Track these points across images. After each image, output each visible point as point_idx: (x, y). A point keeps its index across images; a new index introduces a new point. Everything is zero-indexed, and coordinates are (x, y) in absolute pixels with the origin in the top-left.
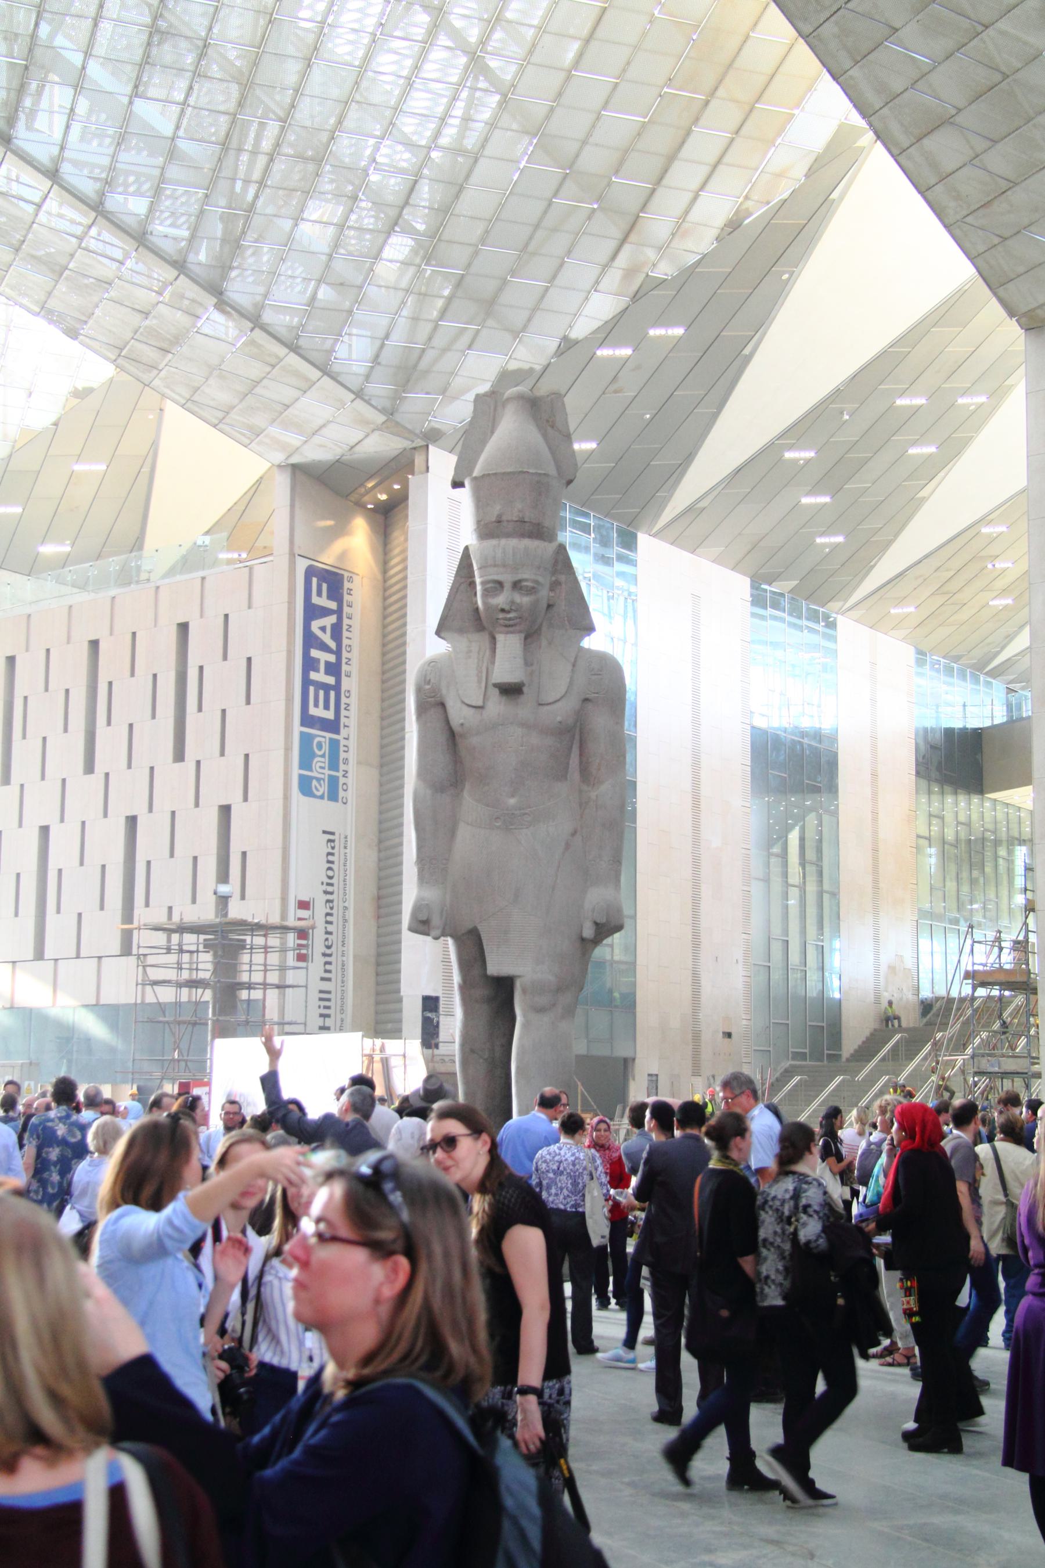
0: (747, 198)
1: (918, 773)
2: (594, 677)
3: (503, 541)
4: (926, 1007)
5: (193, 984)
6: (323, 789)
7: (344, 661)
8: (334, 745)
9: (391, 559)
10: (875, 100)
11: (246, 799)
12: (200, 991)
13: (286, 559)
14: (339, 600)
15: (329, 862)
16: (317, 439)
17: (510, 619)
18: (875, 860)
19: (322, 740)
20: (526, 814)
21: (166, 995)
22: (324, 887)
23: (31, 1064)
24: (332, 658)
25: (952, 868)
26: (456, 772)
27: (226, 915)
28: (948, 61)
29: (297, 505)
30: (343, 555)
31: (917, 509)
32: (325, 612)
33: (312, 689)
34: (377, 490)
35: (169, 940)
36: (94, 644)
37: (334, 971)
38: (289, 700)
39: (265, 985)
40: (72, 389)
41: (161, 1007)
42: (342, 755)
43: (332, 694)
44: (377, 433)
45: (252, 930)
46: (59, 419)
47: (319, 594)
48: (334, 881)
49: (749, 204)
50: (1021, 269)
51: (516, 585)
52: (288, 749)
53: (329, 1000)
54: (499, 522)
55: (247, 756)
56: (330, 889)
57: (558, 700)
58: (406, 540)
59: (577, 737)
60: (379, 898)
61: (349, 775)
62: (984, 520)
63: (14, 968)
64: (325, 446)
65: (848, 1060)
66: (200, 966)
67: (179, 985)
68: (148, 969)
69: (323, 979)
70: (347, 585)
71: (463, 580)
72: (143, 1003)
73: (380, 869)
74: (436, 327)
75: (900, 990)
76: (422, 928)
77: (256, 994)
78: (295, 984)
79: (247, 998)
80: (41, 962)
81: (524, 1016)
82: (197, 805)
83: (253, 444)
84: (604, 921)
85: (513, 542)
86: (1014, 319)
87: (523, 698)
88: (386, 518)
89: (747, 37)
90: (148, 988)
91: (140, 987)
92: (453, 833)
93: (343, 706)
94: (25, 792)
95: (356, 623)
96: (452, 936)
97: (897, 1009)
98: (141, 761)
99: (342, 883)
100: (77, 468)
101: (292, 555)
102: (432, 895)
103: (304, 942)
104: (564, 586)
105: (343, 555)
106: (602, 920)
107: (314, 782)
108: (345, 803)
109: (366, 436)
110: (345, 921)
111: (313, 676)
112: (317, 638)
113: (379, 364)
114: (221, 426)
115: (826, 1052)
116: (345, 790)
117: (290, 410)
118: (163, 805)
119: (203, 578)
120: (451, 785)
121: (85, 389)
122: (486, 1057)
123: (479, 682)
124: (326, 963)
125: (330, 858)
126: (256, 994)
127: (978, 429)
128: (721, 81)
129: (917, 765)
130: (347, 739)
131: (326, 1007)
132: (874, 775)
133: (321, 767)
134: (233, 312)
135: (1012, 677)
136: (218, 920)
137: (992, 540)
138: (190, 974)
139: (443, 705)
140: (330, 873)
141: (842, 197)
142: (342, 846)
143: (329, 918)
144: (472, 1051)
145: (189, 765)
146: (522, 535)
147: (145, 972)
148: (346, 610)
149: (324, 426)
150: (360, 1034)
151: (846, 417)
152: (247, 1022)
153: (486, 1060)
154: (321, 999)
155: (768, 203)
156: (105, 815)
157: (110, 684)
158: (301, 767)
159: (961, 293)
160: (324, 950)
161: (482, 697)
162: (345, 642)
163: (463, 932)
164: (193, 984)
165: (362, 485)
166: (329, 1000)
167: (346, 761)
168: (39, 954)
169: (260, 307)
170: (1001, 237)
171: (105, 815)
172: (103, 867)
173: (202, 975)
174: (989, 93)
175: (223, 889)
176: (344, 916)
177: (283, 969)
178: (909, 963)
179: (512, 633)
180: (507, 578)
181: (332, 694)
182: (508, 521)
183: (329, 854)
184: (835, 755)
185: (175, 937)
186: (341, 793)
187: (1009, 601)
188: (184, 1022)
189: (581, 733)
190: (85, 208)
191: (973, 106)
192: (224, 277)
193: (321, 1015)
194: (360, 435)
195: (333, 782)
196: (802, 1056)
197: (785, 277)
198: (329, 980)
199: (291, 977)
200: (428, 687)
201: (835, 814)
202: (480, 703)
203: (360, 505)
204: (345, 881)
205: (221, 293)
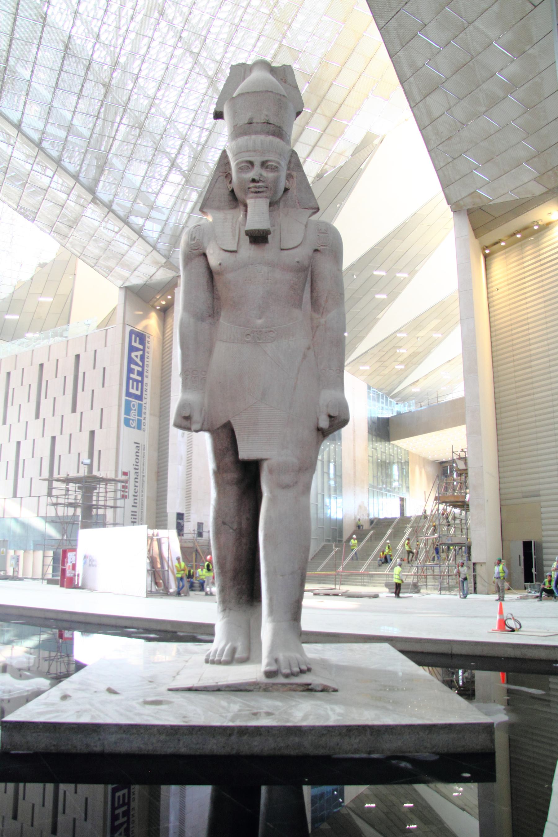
0: (326, 164)
2: (321, 235)
3: (253, 137)
4: (372, 522)
6: (135, 424)
7: (145, 371)
8: (140, 406)
9: (166, 334)
10: (408, 72)
11: (101, 428)
13: (121, 326)
15: (137, 456)
16: (136, 273)
17: (259, 187)
18: (354, 464)
19: (135, 403)
20: (271, 331)
21: (61, 511)
24: (140, 369)
25: (380, 469)
26: (213, 307)
28: (447, 47)
29: (127, 304)
30: (146, 327)
31: (376, 323)
32: (138, 350)
33: (131, 381)
34: (160, 299)
36: (42, 365)
37: (138, 503)
38: (121, 385)
39: (105, 507)
40: (38, 263)
42: (144, 411)
43: (140, 384)
44: (162, 268)
45: (100, 481)
46: (33, 276)
47: (135, 342)
48: (139, 464)
49: (327, 167)
50: (458, 177)
51: (264, 164)
52: (120, 406)
53: (135, 515)
54: (251, 123)
55: (102, 409)
56: (137, 467)
57: (296, 247)
58: (173, 321)
59: (309, 279)
60: (158, 472)
61: (147, 419)
62: (399, 331)
63: (5, 500)
64: (139, 277)
69: (133, 506)
70: (147, 339)
71: (221, 174)
73: (159, 460)
74: (189, 217)
75: (363, 515)
76: (185, 423)
77: (101, 512)
79: (64, 491)
80: (15, 499)
81: (271, 492)
82: (81, 431)
83: (109, 277)
85: (261, 138)
86: (449, 206)
88: (165, 314)
89: (332, 84)
92: (210, 352)
93: (144, 390)
94: (12, 427)
95: (151, 355)
97: (361, 523)
98: (58, 413)
99: (142, 465)
100: (41, 299)
101: (124, 324)
102: (193, 397)
104: (295, 179)
105: (146, 327)
107: (131, 421)
108: (144, 431)
109: (157, 270)
110: (143, 481)
111: (132, 376)
112: (134, 360)
113: (164, 233)
114: (95, 267)
115: (337, 539)
116: (144, 426)
117: (125, 257)
118: (66, 431)
120: (210, 316)
121: (44, 263)
123: (234, 236)
125: (138, 454)
126: (101, 512)
127: (403, 289)
128: (319, 105)
129: (368, 428)
130: (145, 404)
131: (134, 518)
133: (134, 415)
134: (100, 203)
135: (399, 399)
137: (401, 339)
139: (205, 255)
140: (137, 461)
141: (365, 169)
142: (143, 449)
143: (136, 480)
144: (224, 523)
146: (268, 133)
148: (147, 349)
149: (139, 266)
151: (355, 277)
153: (235, 530)
154: (132, 515)
155: (335, 167)
156: (43, 436)
157: (47, 381)
159: (405, 223)
160: (134, 493)
161: (236, 244)
162: (146, 363)
163: (218, 426)
165: (154, 297)
166: (135, 515)
167: (145, 413)
168: (15, 495)
169: (112, 202)
170: (453, 158)
171: (43, 436)
172: (42, 458)
174: (463, 68)
176: (143, 479)
178: (366, 505)
179: (260, 197)
180: (257, 160)
181: (140, 384)
182: (257, 123)
183: (137, 452)
186: (143, 427)
189: (312, 272)
190: (33, 145)
191: (454, 77)
192: (96, 185)
194: (154, 270)
195: (139, 422)
197: (338, 205)
198: (136, 506)
202: (234, 249)
203: (154, 307)
204: (143, 464)
205: (95, 193)
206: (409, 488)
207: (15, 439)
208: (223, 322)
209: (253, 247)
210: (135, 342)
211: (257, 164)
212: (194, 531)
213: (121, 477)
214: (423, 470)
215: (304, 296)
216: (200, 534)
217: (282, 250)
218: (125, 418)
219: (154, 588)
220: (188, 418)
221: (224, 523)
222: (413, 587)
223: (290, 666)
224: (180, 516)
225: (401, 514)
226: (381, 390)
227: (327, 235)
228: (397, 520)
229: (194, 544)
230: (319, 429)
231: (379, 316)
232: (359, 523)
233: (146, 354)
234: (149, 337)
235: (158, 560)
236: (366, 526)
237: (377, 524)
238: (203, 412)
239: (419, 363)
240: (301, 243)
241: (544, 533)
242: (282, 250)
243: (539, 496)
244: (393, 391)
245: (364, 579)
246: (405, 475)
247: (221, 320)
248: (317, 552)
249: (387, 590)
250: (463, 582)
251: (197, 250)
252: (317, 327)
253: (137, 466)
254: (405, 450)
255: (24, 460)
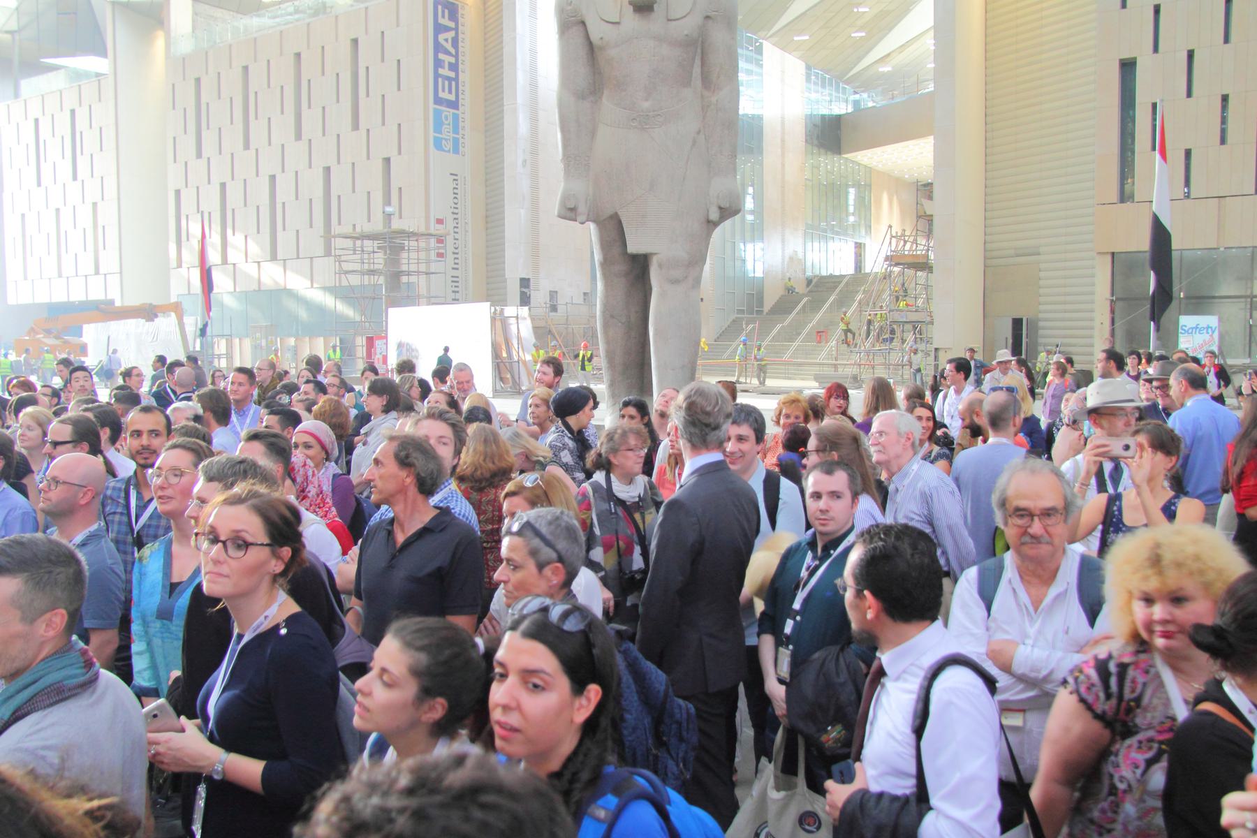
1: (806, 141)
4: (809, 282)
5: (372, 272)
6: (449, 146)
7: (460, 62)
8: (456, 117)
11: (400, 153)
12: (376, 277)
14: (457, 24)
15: (455, 193)
21: (355, 280)
22: (453, 210)
23: (272, 325)
27: (390, 227)
32: (447, 29)
33: (440, 80)
35: (355, 244)
39: (418, 273)
41: (352, 288)
42: (461, 124)
43: (453, 83)
47: (443, 16)
52: (426, 119)
53: (458, 282)
56: (456, 211)
57: (685, 17)
59: (699, 51)
60: (487, 217)
65: (767, 314)
66: (376, 261)
67: (363, 273)
68: (343, 264)
69: (453, 269)
70: (460, 12)
72: (340, 286)
76: (569, 214)
78: (437, 271)
84: (728, 205)
87: (654, 15)
90: (343, 276)
91: (337, 275)
92: (593, 134)
93: (460, 92)
96: (594, 221)
103: (440, 245)
106: (725, 204)
107: (444, 141)
110: (466, 231)
112: (442, 46)
119: (366, 8)
122: (623, 321)
124: (455, 258)
125: (455, 191)
126: (413, 279)
129: (806, 135)
131: (456, 287)
132: (783, 141)
135: (857, 84)
136: (386, 230)
138: (369, 266)
139: (583, 23)
140: (456, 201)
144: (612, 316)
145: (363, 132)
147: (340, 265)
150: (488, 303)
152: (408, 296)
154: (453, 281)
158: (435, 132)
162: (461, 49)
164: (372, 272)
166: (458, 282)
167: (463, 128)
173: (376, 267)
175: (389, 209)
177: (428, 262)
178: (800, 255)
181: (453, 83)
184: (761, 128)
185: (359, 243)
187: (863, 34)
188: (367, 298)
193: (453, 292)
195: (456, 142)
196: (741, 311)
198: (457, 269)
199: (433, 268)
200: (569, 8)
201: (762, 165)
202: (617, 20)
206: (870, 227)
207: (266, 171)
208: (607, 103)
209: (637, 16)
210: (443, 16)
212: (545, 303)
213: (435, 228)
214: (895, 198)
215: (694, 72)
216: (554, 308)
217: (669, 20)
218: (435, 138)
219: (500, 385)
220: (573, 210)
221: (612, 316)
222: (852, 380)
224: (525, 283)
225: (856, 268)
226: (827, 72)
228: (845, 280)
229: (547, 322)
230: (709, 221)
232: (789, 284)
233: (461, 36)
234: (463, 8)
235: (504, 347)
236: (801, 288)
237: (817, 285)
239: (890, 28)
240: (691, 11)
241: (1042, 307)
242: (669, 20)
243: (1039, 254)
244: (847, 73)
245: (788, 369)
246: (864, 205)
247: (604, 100)
248: (724, 329)
249: (817, 384)
250: (915, 375)
252: (708, 106)
253: (457, 208)
254: (866, 166)
255: (284, 203)
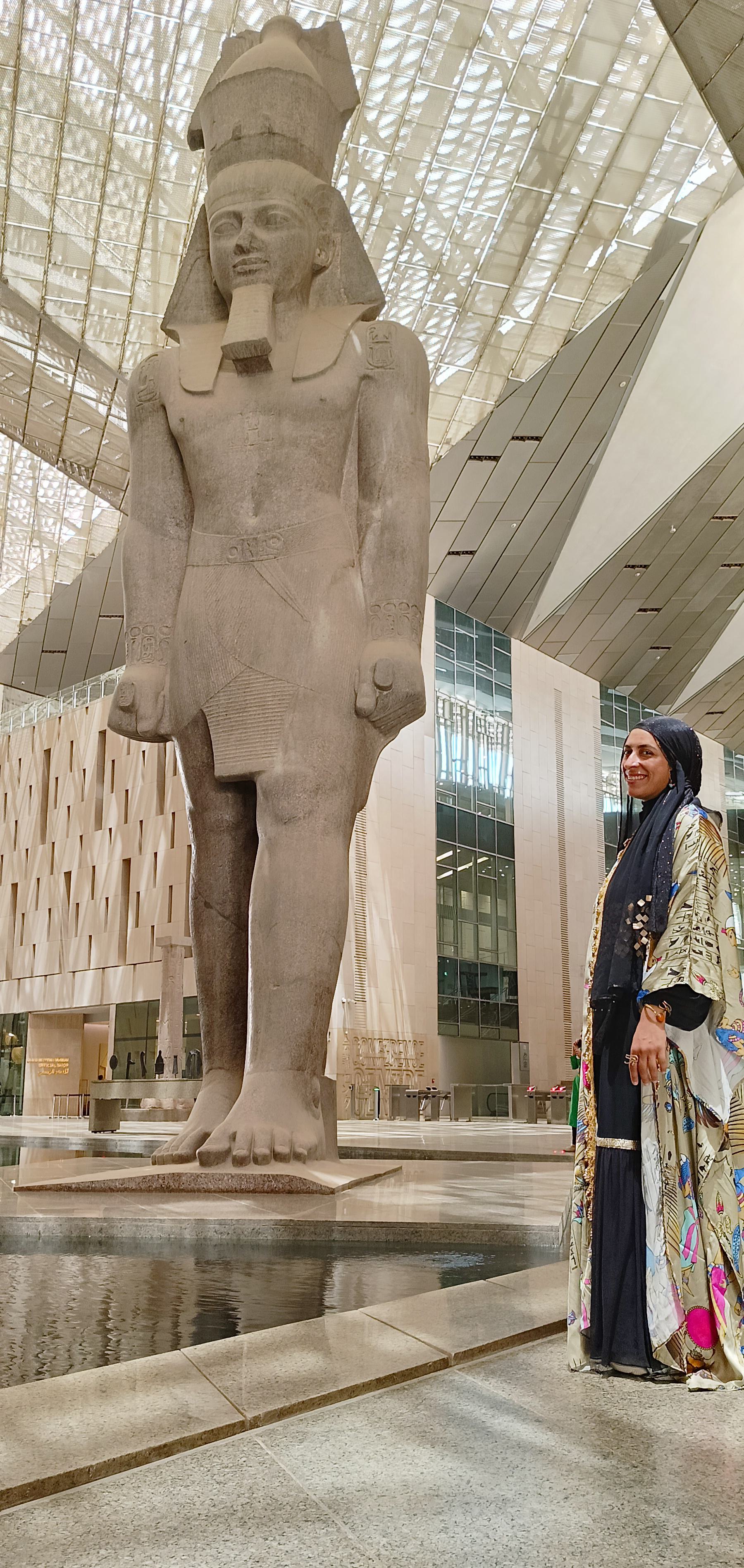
104: (338, 247)
211: (247, 216)
217: (294, 380)
223: (252, 1143)
227: (388, 345)
231: (732, 607)
238: (161, 698)
251: (149, 400)
